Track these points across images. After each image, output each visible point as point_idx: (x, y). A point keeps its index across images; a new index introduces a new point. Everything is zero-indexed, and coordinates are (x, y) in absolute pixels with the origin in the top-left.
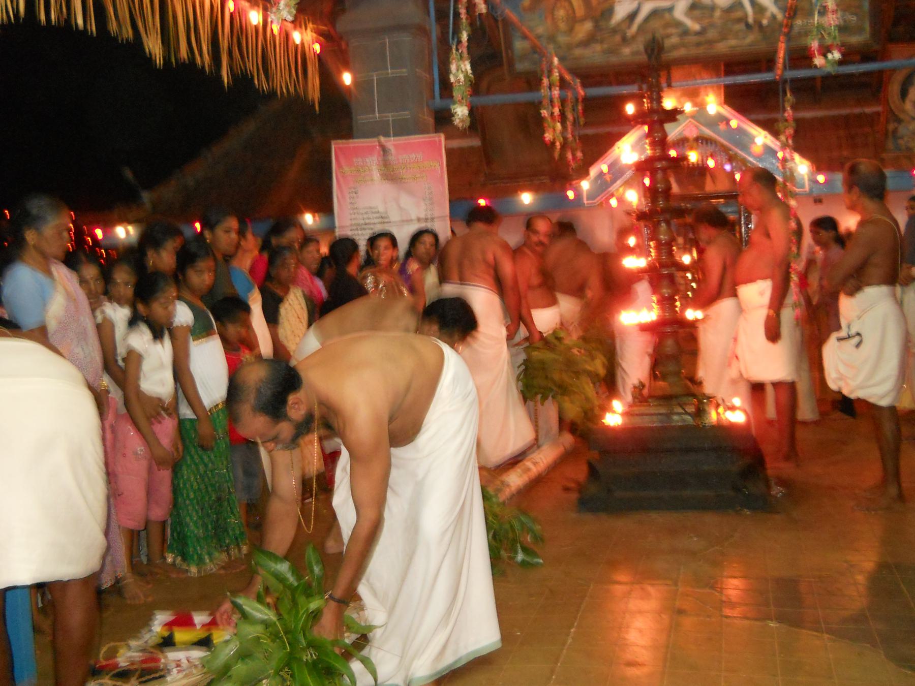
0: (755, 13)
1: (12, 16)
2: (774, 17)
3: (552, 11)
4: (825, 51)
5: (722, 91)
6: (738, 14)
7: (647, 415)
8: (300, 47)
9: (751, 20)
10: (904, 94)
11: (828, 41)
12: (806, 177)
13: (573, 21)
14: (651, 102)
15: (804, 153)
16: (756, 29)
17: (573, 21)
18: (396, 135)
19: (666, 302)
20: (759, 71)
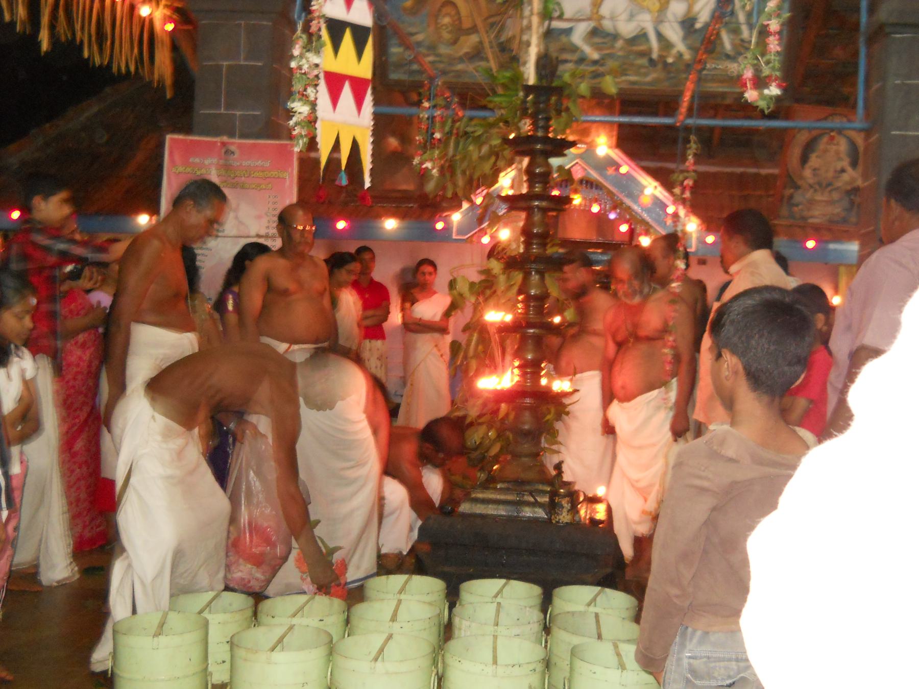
1: (452, 145)
2: (680, 55)
3: (436, 16)
4: (760, 82)
5: (615, 133)
6: (642, 48)
8: (147, 23)
9: (655, 56)
10: (804, 159)
11: (766, 71)
12: (694, 236)
13: (459, 31)
16: (660, 66)
17: (459, 31)
18: (243, 136)
19: (531, 369)
20: (655, 114)
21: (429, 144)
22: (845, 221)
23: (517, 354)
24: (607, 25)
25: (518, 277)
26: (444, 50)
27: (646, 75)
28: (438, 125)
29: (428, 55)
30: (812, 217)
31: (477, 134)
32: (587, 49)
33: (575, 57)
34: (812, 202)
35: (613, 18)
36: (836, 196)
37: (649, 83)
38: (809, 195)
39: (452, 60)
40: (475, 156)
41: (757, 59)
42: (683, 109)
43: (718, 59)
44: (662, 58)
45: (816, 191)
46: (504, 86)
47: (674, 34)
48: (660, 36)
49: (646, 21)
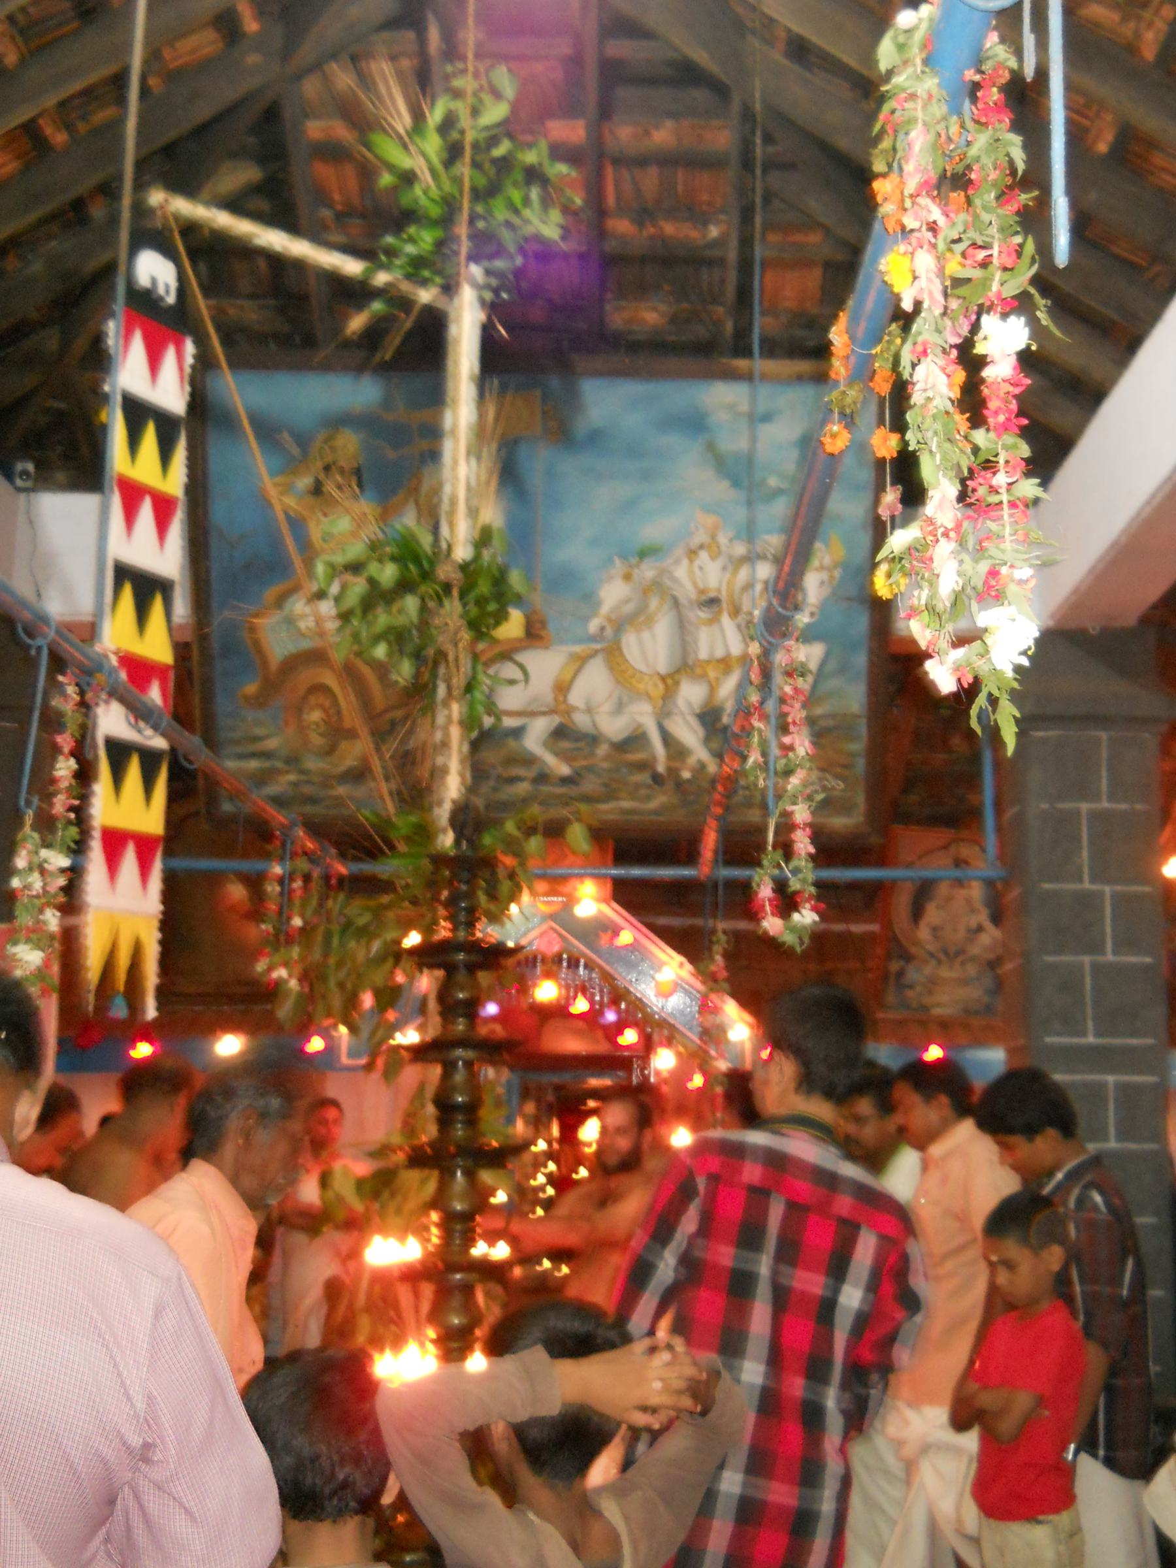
0: (670, 757)
2: (702, 766)
3: (299, 709)
4: (787, 903)
9: (661, 768)
10: (917, 912)
13: (337, 733)
14: (455, 929)
16: (670, 785)
17: (337, 733)
21: (282, 938)
22: (988, 1009)
23: (435, 1316)
24: (581, 721)
26: (312, 764)
27: (649, 798)
28: (297, 902)
29: (287, 772)
30: (938, 1005)
32: (550, 760)
33: (531, 773)
34: (933, 983)
35: (589, 710)
37: (656, 812)
38: (928, 970)
39: (327, 780)
40: (361, 956)
41: (779, 866)
44: (673, 772)
45: (940, 962)
46: (408, 839)
47: (689, 734)
48: (667, 739)
49: (643, 715)
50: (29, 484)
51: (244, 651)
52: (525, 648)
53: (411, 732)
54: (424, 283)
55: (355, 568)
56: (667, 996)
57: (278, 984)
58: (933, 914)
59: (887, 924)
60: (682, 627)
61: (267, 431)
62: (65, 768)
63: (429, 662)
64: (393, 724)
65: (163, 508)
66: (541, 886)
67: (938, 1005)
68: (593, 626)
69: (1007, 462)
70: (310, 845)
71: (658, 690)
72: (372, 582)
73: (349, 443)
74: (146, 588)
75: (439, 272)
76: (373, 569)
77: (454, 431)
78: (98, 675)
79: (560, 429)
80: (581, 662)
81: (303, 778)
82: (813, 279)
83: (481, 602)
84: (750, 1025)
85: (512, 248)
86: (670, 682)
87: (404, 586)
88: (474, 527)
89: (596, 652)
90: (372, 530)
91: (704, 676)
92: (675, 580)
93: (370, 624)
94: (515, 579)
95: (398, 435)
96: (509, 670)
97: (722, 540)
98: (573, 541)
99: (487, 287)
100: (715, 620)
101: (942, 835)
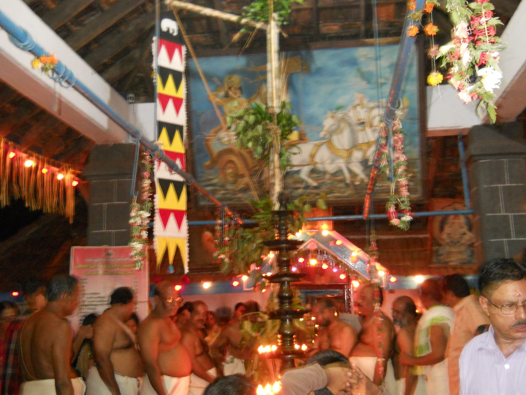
3: (224, 168)
4: (399, 212)
6: (340, 178)
7: (323, 286)
9: (348, 181)
10: (442, 229)
13: (238, 176)
15: (383, 264)
17: (238, 176)
18: (117, 245)
21: (222, 244)
24: (319, 167)
25: (278, 322)
26: (230, 187)
27: (344, 192)
29: (220, 190)
30: (452, 261)
31: (248, 237)
33: (303, 186)
34: (449, 253)
35: (322, 163)
36: (463, 248)
39: (235, 192)
42: (366, 209)
43: (383, 180)
44: (353, 182)
46: (264, 209)
47: (358, 169)
49: (341, 163)
50: (134, 101)
51: (205, 149)
52: (299, 143)
53: (261, 174)
54: (258, 21)
55: (240, 118)
56: (355, 262)
57: (222, 260)
58: (447, 229)
59: (432, 234)
60: (353, 133)
61: (209, 77)
62: (146, 183)
63: (267, 148)
64: (257, 171)
65: (177, 103)
66: (309, 226)
67: (452, 261)
68: (322, 134)
69: (485, 13)
70: (229, 213)
71: (345, 154)
72: (247, 122)
73: (236, 79)
74: (172, 129)
75: (263, 17)
76: (246, 117)
77: (271, 71)
78: (157, 152)
79: (306, 68)
80: (318, 146)
81: (226, 192)
82: (391, 9)
83: (284, 126)
84: (385, 271)
85: (287, 7)
86: (350, 152)
87: (257, 123)
88: (279, 102)
89: (322, 144)
90: (245, 105)
91: (361, 149)
92: (349, 117)
93: (246, 136)
94: (294, 118)
95: (253, 75)
96: (295, 150)
97: (365, 102)
98: (314, 105)
99: (279, 21)
100: (363, 130)
101: (449, 201)
